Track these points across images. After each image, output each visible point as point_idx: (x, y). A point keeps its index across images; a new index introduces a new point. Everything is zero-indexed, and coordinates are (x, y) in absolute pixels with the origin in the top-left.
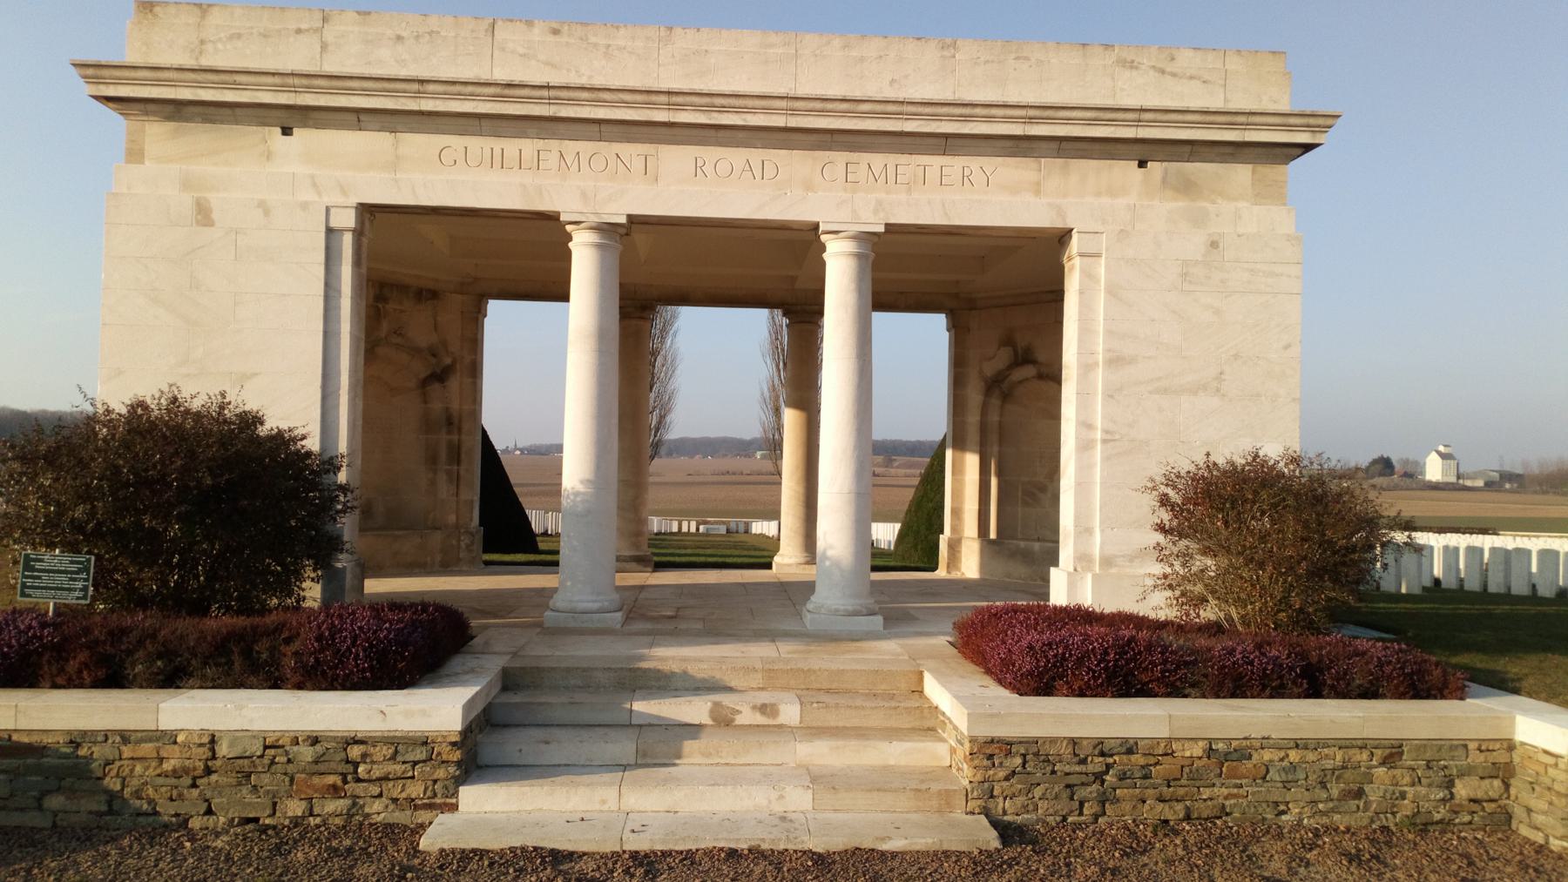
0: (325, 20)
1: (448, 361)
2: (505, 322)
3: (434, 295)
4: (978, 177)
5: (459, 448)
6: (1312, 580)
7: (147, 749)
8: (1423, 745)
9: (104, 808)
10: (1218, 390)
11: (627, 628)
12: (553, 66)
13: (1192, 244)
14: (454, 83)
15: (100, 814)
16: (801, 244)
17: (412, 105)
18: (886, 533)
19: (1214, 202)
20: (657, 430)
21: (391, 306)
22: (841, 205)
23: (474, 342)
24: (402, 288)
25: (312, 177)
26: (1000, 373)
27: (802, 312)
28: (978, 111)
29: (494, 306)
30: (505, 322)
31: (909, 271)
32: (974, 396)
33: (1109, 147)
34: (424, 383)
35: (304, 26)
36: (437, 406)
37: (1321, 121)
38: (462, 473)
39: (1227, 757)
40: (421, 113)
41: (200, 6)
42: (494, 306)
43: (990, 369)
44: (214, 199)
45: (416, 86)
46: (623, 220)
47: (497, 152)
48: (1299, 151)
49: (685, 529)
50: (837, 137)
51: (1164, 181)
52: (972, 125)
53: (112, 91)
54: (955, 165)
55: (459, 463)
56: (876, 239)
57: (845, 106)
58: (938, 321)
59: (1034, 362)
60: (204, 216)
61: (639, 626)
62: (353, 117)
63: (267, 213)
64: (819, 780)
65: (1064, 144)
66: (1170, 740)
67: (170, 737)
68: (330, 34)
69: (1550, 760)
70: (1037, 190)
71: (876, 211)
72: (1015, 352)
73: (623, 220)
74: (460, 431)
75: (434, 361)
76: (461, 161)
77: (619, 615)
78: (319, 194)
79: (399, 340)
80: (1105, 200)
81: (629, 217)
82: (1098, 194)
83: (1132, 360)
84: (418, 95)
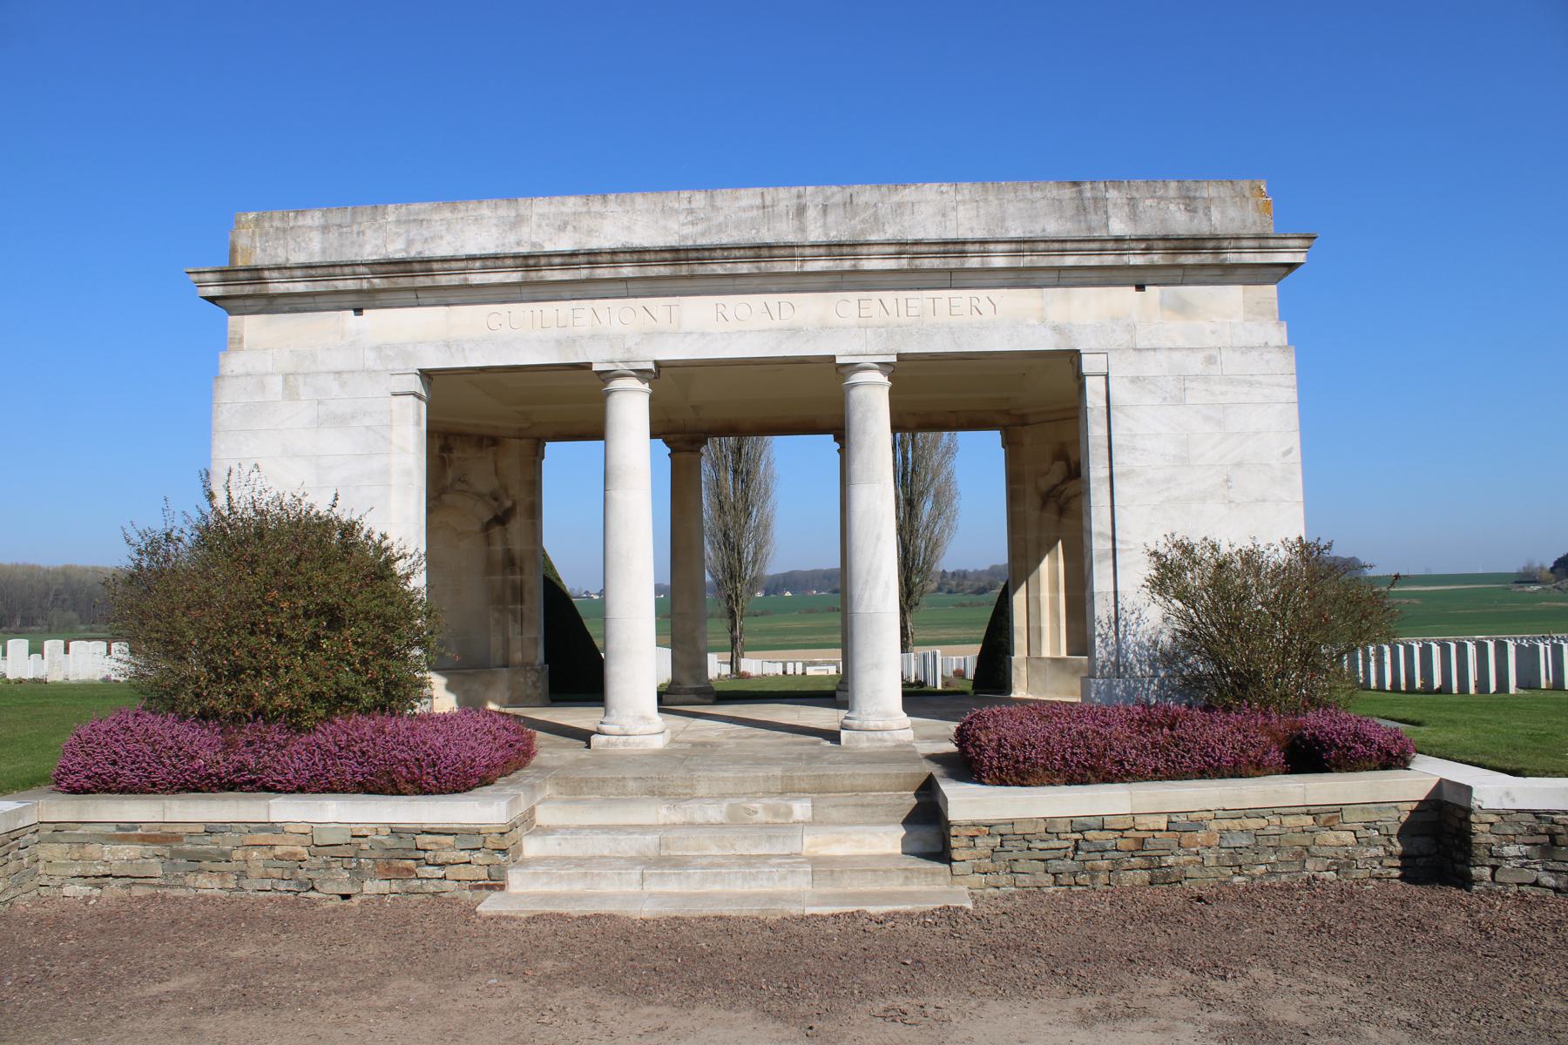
1: (508, 504)
3: (495, 441)
4: (985, 306)
7: (261, 838)
20: (755, 562)
21: (455, 455)
23: (534, 486)
24: (464, 436)
29: (551, 448)
31: (937, 398)
34: (487, 527)
39: (1181, 827)
42: (551, 448)
43: (1045, 484)
48: (1284, 270)
49: (790, 671)
51: (1162, 303)
55: (522, 602)
58: (995, 437)
62: (412, 295)
64: (823, 867)
65: (1063, 274)
72: (1068, 465)
74: (522, 570)
75: (495, 504)
79: (464, 486)
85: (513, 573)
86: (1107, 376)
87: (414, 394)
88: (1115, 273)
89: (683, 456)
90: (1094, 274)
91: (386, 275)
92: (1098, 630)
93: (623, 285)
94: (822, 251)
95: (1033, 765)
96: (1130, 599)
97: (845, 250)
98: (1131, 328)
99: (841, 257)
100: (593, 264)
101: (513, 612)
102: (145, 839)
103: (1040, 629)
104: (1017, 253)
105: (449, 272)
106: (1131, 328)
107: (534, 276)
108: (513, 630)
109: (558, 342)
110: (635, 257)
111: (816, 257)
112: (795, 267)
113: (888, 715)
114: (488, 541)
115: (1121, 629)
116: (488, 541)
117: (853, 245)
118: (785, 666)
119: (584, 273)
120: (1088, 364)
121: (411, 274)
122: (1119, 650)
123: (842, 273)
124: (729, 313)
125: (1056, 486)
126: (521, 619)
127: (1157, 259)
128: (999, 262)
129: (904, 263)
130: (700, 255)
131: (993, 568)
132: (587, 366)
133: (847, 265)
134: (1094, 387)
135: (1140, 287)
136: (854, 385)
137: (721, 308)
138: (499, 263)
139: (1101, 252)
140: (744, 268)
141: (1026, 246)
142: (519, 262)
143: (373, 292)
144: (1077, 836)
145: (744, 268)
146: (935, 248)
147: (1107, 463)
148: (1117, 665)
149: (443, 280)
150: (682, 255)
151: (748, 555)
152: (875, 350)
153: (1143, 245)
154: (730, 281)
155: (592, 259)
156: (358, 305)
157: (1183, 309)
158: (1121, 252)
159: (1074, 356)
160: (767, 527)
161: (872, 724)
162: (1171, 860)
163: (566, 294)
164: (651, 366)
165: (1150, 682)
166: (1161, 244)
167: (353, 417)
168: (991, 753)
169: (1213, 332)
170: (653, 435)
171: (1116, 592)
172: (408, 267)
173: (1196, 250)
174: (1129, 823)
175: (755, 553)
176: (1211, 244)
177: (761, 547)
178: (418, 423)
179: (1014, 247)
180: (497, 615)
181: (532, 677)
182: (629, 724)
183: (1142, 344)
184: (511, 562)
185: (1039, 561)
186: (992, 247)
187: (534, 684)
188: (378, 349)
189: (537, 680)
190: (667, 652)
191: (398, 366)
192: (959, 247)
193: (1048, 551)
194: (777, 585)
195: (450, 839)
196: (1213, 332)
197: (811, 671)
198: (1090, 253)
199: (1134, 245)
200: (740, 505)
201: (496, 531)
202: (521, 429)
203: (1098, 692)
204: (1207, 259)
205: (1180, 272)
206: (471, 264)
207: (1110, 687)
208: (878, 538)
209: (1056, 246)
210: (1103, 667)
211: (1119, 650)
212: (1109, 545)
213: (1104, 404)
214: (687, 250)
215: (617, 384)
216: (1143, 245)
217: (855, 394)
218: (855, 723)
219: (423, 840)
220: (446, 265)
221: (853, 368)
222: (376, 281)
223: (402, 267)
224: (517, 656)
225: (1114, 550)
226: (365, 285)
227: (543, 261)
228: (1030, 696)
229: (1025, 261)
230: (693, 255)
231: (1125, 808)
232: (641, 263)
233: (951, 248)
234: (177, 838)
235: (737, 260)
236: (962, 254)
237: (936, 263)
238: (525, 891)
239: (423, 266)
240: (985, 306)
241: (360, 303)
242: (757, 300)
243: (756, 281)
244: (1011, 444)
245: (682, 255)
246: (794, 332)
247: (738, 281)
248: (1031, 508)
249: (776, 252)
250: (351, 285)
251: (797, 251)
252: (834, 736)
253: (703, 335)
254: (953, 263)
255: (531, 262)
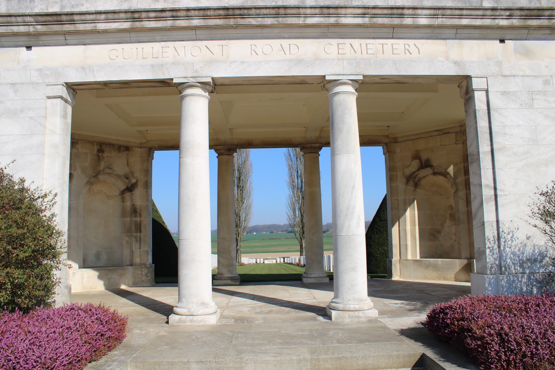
1: (134, 181)
2: (458, 264)
3: (127, 149)
4: (413, 49)
20: (245, 221)
21: (106, 154)
23: (148, 172)
24: (111, 145)
30: (458, 264)
34: (123, 193)
38: (142, 237)
43: (408, 172)
49: (258, 262)
55: (140, 232)
59: (431, 166)
62: (62, 38)
65: (459, 31)
74: (140, 216)
75: (127, 181)
79: (110, 171)
85: (136, 217)
86: (487, 91)
87: (61, 97)
88: (489, 31)
89: (225, 157)
90: (477, 31)
91: (44, 24)
92: (488, 245)
93: (193, 32)
94: (317, 11)
95: (540, 360)
96: (507, 225)
97: (331, 11)
98: (499, 64)
99: (329, 15)
100: (175, 18)
101: (136, 237)
103: (406, 245)
104: (435, 16)
105: (84, 22)
106: (499, 64)
107: (138, 24)
108: (135, 246)
109: (153, 66)
110: (201, 13)
111: (313, 15)
112: (300, 21)
113: (361, 300)
115: (502, 244)
117: (336, 8)
118: (256, 260)
119: (169, 23)
120: (476, 83)
121: (61, 23)
122: (500, 257)
123: (328, 26)
124: (259, 51)
125: (414, 173)
126: (140, 241)
127: (515, 22)
128: (423, 21)
129: (366, 20)
130: (242, 12)
131: (327, 224)
133: (332, 20)
134: (479, 98)
135: (502, 41)
136: (337, 93)
137: (253, 47)
138: (116, 16)
139: (483, 17)
140: (269, 21)
141: (440, 12)
142: (129, 15)
143: (37, 35)
145: (269, 21)
146: (386, 11)
147: (489, 143)
148: (500, 266)
149: (81, 27)
150: (231, 12)
151: (243, 218)
152: (349, 73)
153: (508, 13)
154: (259, 31)
155: (175, 14)
156: (29, 44)
157: (527, 54)
158: (494, 17)
159: (468, 78)
160: (250, 207)
161: (352, 307)
163: (158, 38)
164: (210, 80)
165: (522, 277)
166: (518, 13)
167: (22, 111)
168: (497, 347)
169: (546, 67)
170: (211, 147)
171: (498, 221)
172: (59, 18)
173: (538, 17)
175: (245, 217)
176: (547, 13)
177: (248, 215)
178: (65, 116)
179: (432, 12)
180: (127, 238)
181: (145, 271)
182: (194, 308)
183: (507, 73)
184: (135, 211)
185: (405, 211)
186: (419, 12)
187: (146, 274)
188: (40, 70)
189: (148, 273)
190: (216, 256)
191: (52, 80)
192: (400, 11)
193: (409, 205)
194: (256, 229)
196: (546, 67)
197: (266, 262)
198: (477, 17)
199: (502, 13)
200: (240, 199)
201: (127, 195)
202: (141, 143)
203: (490, 284)
204: (544, 22)
205: (526, 31)
206: (98, 17)
207: (497, 280)
208: (353, 187)
209: (458, 12)
210: (492, 268)
211: (500, 257)
212: (492, 192)
213: (486, 108)
214: (234, 9)
215: (188, 91)
216: (508, 13)
217: (337, 99)
218: (340, 306)
220: (83, 17)
221: (336, 83)
222: (39, 27)
223: (55, 18)
224: (137, 260)
225: (496, 196)
226: (31, 29)
227: (144, 15)
228: (402, 280)
229: (439, 21)
230: (237, 12)
232: (205, 17)
233: (395, 11)
235: (264, 16)
236: (402, 16)
237: (386, 21)
239: (68, 18)
240: (413, 49)
241: (30, 41)
242: (276, 43)
243: (276, 31)
244: (389, 153)
245: (231, 12)
246: (299, 61)
247: (265, 31)
248: (400, 184)
249: (289, 11)
250: (22, 29)
251: (302, 11)
252: (323, 312)
253: (243, 62)
254: (396, 21)
255: (136, 15)
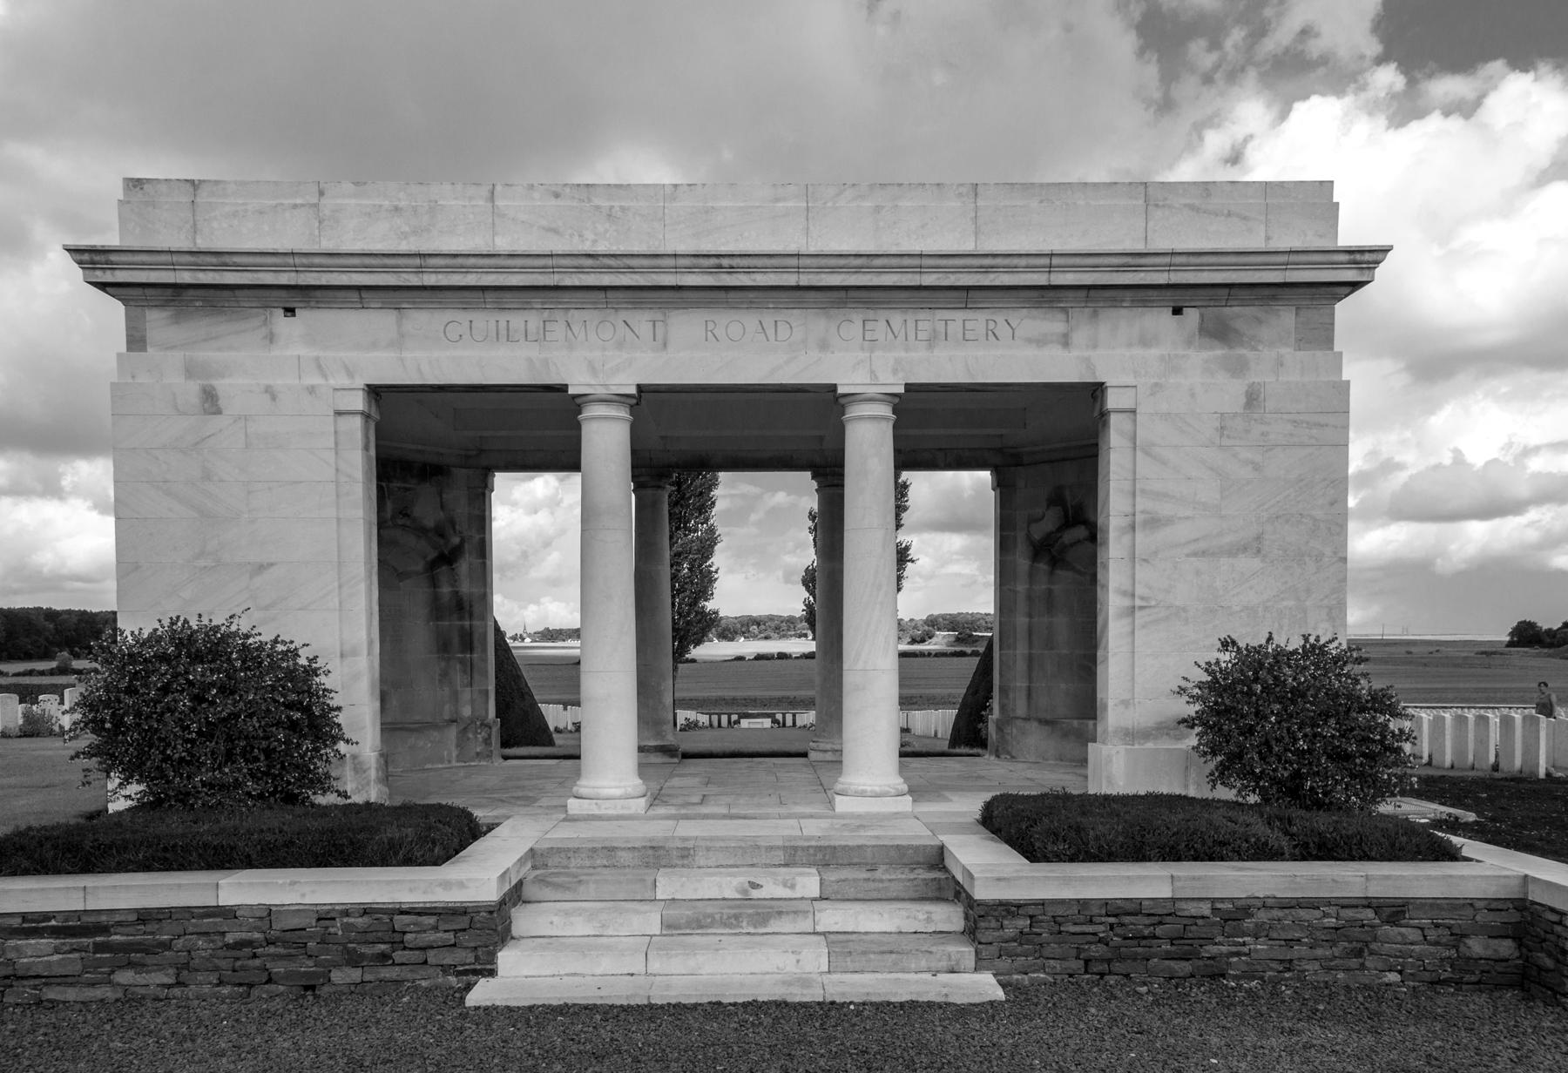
0: (321, 193)
1: (456, 540)
5: (471, 634)
6: (1301, 739)
8: (1433, 904)
9: (171, 981)
10: (1259, 551)
11: (651, 812)
12: (555, 231)
13: (1228, 393)
14: (455, 256)
15: (169, 986)
16: (827, 405)
17: (414, 280)
18: (937, 722)
19: (1254, 349)
22: (868, 363)
23: (481, 520)
25: (317, 359)
26: (1049, 535)
27: (830, 473)
28: (999, 261)
31: (936, 428)
32: (1022, 562)
33: (1141, 294)
34: (433, 565)
35: (299, 201)
36: (445, 590)
37: (1367, 257)
39: (1234, 915)
40: (424, 288)
41: (192, 182)
43: (1039, 531)
44: (221, 385)
45: (417, 261)
46: (633, 391)
47: (503, 324)
48: (1347, 290)
50: (852, 294)
52: (992, 276)
53: (108, 277)
54: (977, 320)
56: (897, 400)
57: (859, 262)
60: (211, 401)
61: (661, 811)
63: (274, 398)
66: (1174, 900)
67: (229, 913)
68: (328, 203)
69: (1554, 918)
70: (1065, 341)
71: (895, 372)
73: (633, 391)
76: (466, 336)
77: (643, 800)
78: (325, 377)
80: (1138, 351)
81: (639, 387)
82: (1130, 345)
83: (1169, 521)
84: (420, 270)
85: (461, 618)
89: (649, 492)
101: (462, 661)
102: (56, 932)
114: (434, 583)
116: (434, 583)
120: (1113, 400)
126: (470, 669)
132: (563, 388)
144: (1112, 920)
162: (1213, 950)
174: (1169, 908)
191: (345, 382)
195: (431, 920)
219: (400, 921)
231: (1164, 892)
234: (104, 929)
238: (522, 975)
